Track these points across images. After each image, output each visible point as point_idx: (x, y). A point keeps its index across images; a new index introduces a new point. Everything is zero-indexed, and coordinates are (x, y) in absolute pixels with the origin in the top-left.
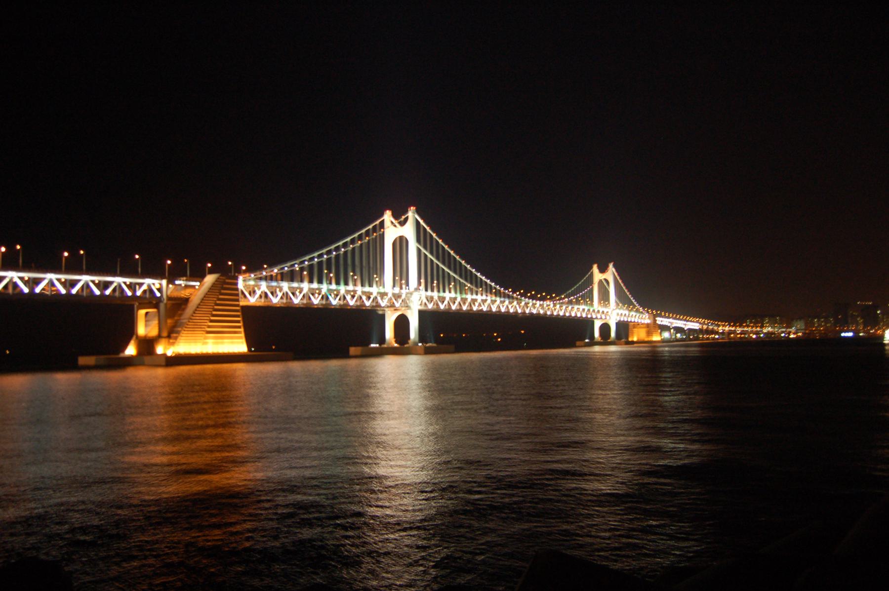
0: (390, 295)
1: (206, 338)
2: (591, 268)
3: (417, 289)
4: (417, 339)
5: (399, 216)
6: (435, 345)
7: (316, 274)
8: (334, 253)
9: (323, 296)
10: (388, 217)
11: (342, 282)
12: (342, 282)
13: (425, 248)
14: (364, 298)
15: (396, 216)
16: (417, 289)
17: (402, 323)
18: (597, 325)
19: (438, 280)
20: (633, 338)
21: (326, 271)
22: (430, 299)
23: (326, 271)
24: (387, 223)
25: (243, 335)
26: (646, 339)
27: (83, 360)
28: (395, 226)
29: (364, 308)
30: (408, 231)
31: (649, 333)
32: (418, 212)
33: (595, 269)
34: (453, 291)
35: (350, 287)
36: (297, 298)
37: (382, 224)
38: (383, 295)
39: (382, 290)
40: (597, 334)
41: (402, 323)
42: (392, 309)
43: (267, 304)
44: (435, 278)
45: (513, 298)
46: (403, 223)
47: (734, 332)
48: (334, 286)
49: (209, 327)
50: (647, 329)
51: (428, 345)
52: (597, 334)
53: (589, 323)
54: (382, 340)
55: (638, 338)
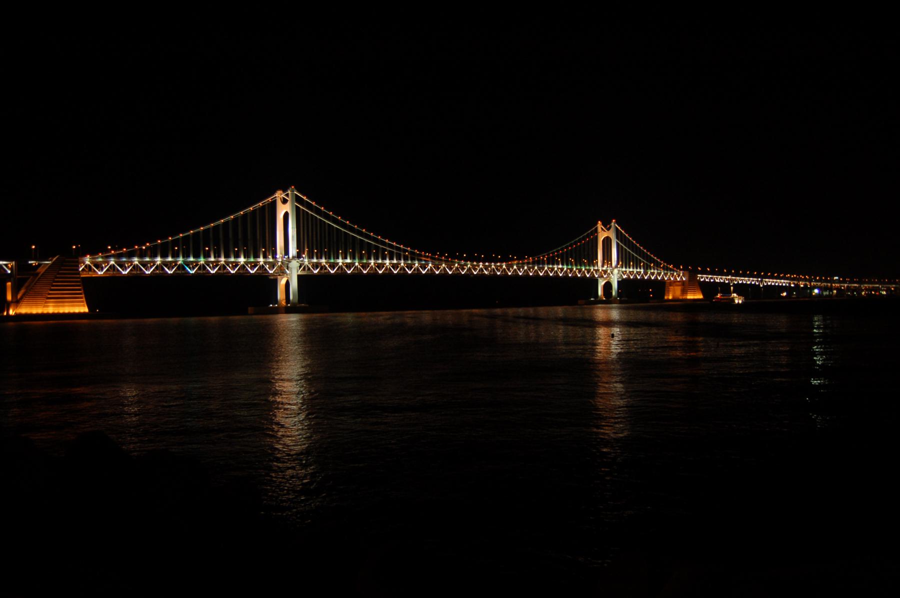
0: (600, 270)
1: (46, 302)
2: (597, 223)
3: (616, 267)
4: (616, 296)
5: (608, 228)
6: (626, 299)
7: (194, 247)
8: (561, 252)
9: (339, 267)
10: (600, 225)
11: (628, 267)
12: (628, 267)
13: (621, 242)
14: (586, 272)
15: (604, 225)
16: (616, 267)
17: (608, 286)
18: (601, 283)
19: (622, 261)
20: (669, 296)
21: (316, 251)
22: (623, 273)
23: (316, 251)
24: (599, 230)
25: (84, 299)
26: (681, 298)
27: (579, 302)
28: (604, 231)
29: (144, 275)
30: (612, 234)
31: (684, 292)
32: (617, 222)
33: (600, 225)
34: (631, 268)
35: (560, 266)
36: (510, 272)
37: (596, 230)
38: (597, 271)
39: (596, 268)
40: (600, 292)
41: (608, 286)
42: (602, 278)
43: (311, 274)
44: (631, 260)
45: (441, 260)
46: (608, 229)
47: (859, 290)
48: (560, 266)
49: (49, 294)
50: (682, 287)
51: (623, 299)
52: (600, 292)
53: (594, 282)
54: (275, 300)
55: (673, 296)
